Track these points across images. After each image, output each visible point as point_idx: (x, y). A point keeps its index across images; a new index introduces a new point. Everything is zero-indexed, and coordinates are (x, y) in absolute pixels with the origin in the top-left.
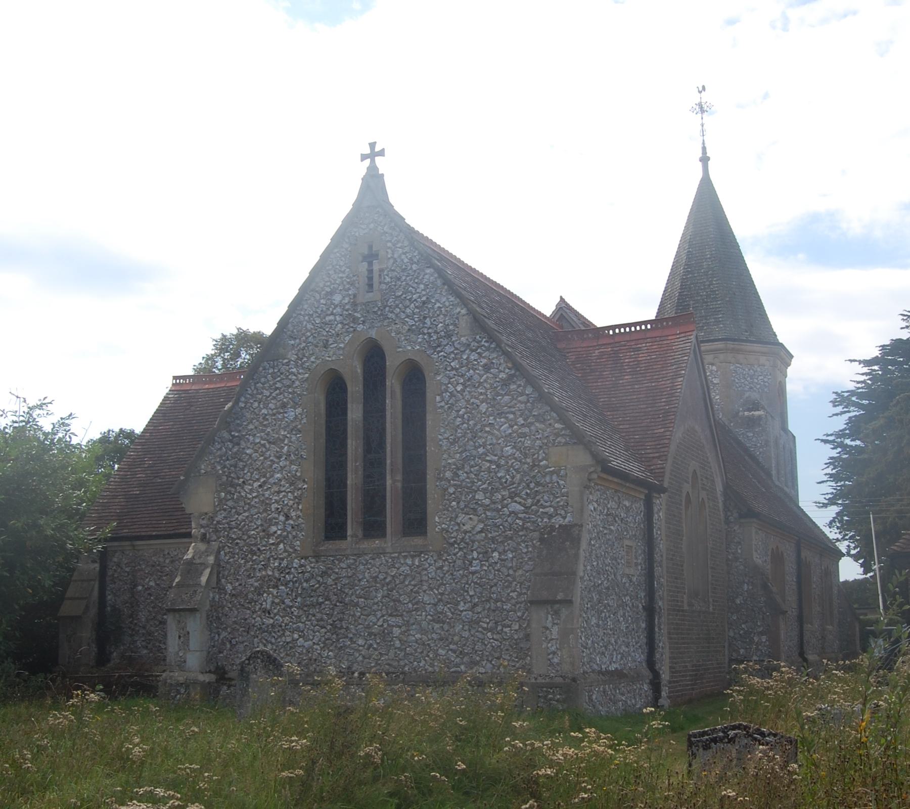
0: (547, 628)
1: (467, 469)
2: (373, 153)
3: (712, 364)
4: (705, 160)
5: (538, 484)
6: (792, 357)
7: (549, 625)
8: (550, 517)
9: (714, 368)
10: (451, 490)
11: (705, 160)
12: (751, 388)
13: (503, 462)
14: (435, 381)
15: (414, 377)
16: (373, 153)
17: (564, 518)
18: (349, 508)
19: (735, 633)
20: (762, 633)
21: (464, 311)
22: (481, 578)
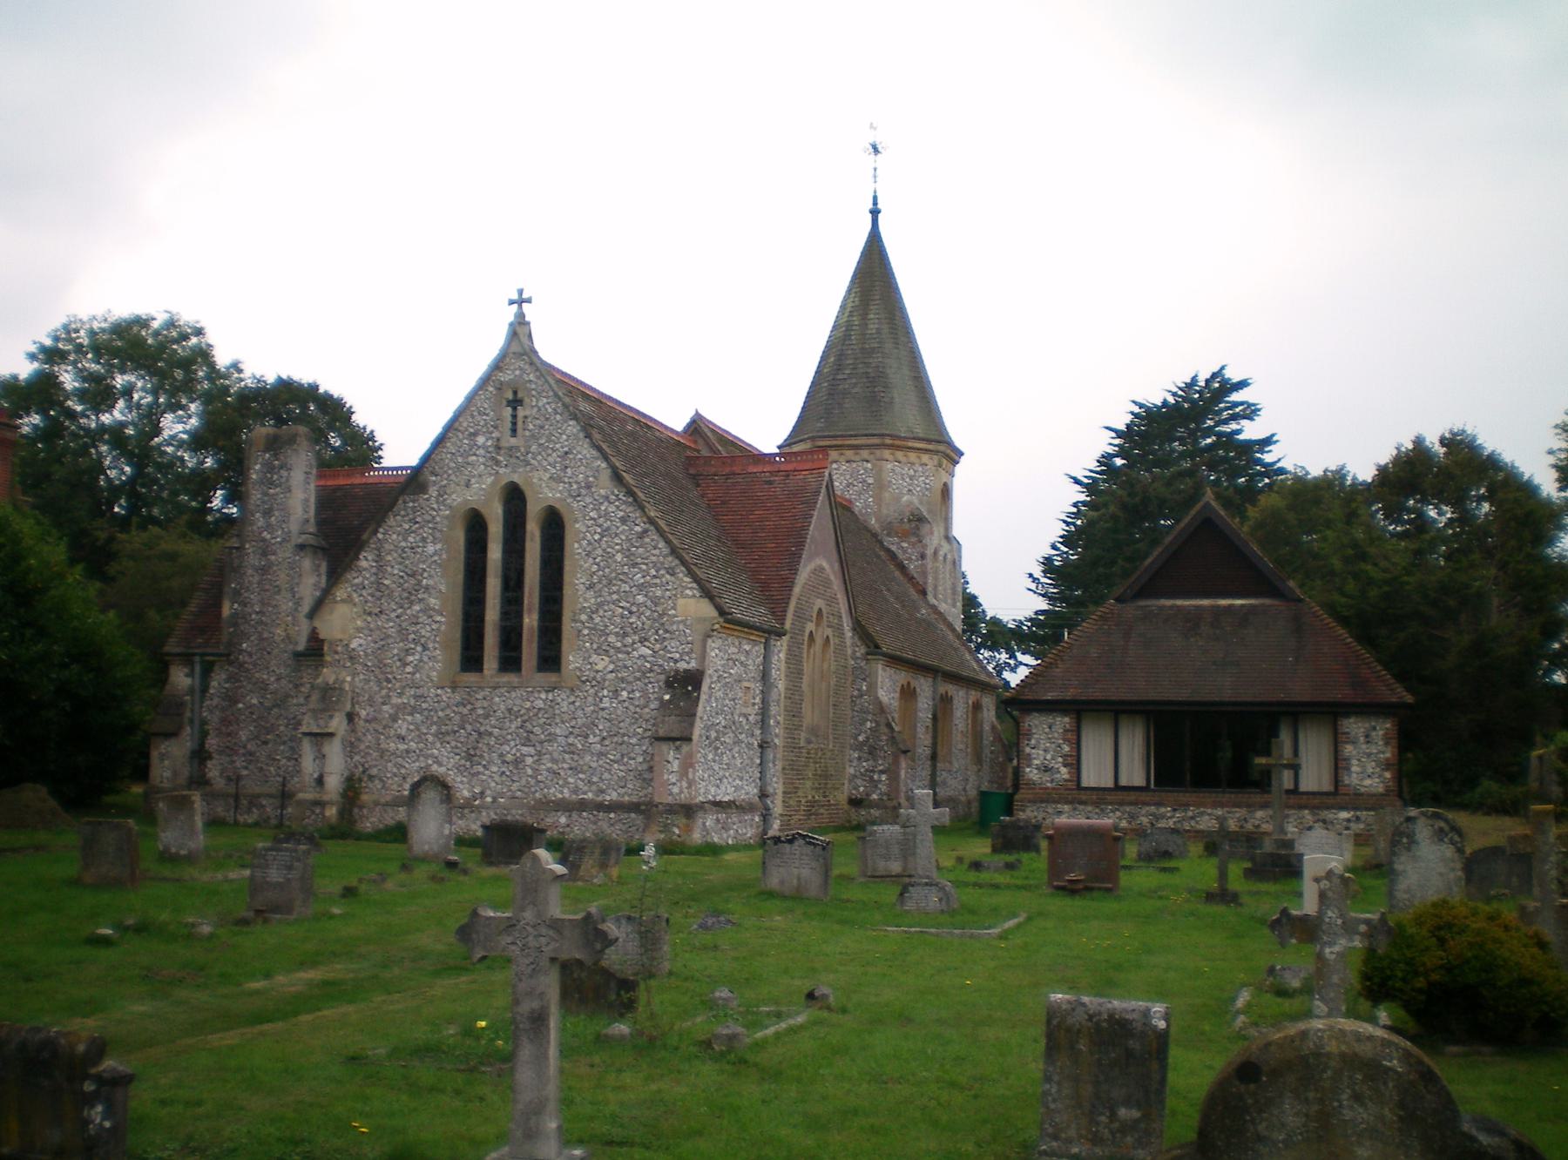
4: (875, 213)
5: (667, 631)
8: (676, 661)
11: (875, 213)
20: (882, 772)
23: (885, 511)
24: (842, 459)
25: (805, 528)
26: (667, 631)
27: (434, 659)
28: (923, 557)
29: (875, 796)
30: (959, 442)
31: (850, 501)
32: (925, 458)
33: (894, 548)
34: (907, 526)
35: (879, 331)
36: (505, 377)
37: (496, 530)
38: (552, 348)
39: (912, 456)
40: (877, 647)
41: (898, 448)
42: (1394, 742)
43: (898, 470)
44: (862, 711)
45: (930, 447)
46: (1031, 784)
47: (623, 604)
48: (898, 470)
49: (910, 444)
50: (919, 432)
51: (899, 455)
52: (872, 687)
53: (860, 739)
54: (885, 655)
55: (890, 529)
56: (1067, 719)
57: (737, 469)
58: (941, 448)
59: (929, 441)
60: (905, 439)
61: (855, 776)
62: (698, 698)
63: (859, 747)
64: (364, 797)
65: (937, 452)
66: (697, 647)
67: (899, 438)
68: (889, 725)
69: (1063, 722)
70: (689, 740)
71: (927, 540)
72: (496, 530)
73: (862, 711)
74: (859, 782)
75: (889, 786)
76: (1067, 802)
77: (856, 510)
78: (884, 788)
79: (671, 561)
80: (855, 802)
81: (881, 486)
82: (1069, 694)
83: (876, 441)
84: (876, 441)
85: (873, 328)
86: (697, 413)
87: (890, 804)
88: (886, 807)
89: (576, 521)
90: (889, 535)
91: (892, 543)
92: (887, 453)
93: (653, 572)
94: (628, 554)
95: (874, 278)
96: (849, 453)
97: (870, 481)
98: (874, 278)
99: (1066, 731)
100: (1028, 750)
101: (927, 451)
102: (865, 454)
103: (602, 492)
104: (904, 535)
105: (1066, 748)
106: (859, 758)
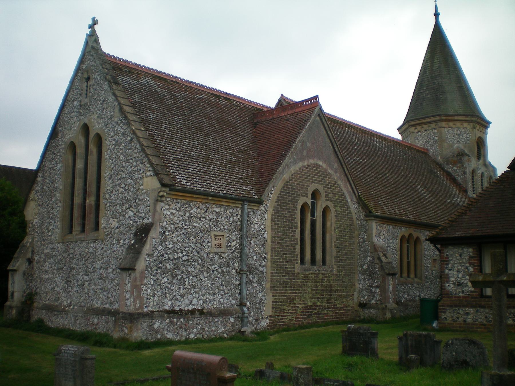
0: (125, 284)
1: (114, 193)
2: (95, 22)
3: (435, 129)
4: (437, 15)
5: (140, 200)
6: (489, 123)
7: (127, 283)
8: (143, 219)
9: (436, 131)
10: (108, 205)
11: (437, 15)
12: (458, 141)
13: (127, 188)
14: (107, 143)
15: (99, 140)
16: (95, 22)
17: (148, 219)
18: (299, 214)
19: (363, 286)
20: (377, 287)
21: (117, 104)
22: (116, 255)
23: (445, 153)
24: (423, 130)
25: (293, 141)
26: (140, 200)
27: (57, 228)
28: (464, 173)
29: (373, 302)
30: (488, 118)
31: (427, 150)
32: (466, 125)
33: (450, 170)
34: (455, 159)
35: (439, 67)
36: (84, 67)
37: (80, 151)
38: (108, 47)
39: (458, 124)
40: (370, 212)
41: (449, 121)
42: (21, 244)
43: (451, 132)
44: (365, 251)
45: (468, 119)
46: (449, 295)
47: (123, 185)
48: (451, 132)
49: (456, 118)
50: (461, 112)
51: (451, 124)
52: (370, 236)
53: (365, 267)
54: (376, 217)
55: (448, 161)
56: (471, 250)
57: (275, 116)
58: (474, 119)
59: (466, 116)
60: (453, 116)
61: (362, 290)
62: (145, 241)
63: (364, 272)
64: (35, 305)
65: (472, 121)
66: (151, 208)
67: (449, 116)
68: (379, 259)
69: (468, 251)
70: (133, 269)
71: (466, 165)
72: (80, 151)
73: (365, 251)
74: (365, 293)
75: (381, 295)
76: (472, 307)
77: (431, 154)
78: (378, 297)
79: (141, 155)
80: (363, 305)
81: (442, 140)
82: (470, 233)
83: (437, 118)
84: (437, 118)
85: (436, 66)
86: (282, 95)
87: (380, 306)
88: (379, 309)
89: (106, 140)
90: (447, 164)
91: (448, 168)
92: (444, 124)
93: (135, 164)
94: (125, 154)
95: (439, 47)
96: (426, 127)
97: (437, 138)
98: (439, 47)
99: (470, 257)
100: (447, 271)
101: (466, 121)
102: (433, 125)
103: (116, 120)
104: (454, 163)
105: (471, 269)
106: (364, 279)
